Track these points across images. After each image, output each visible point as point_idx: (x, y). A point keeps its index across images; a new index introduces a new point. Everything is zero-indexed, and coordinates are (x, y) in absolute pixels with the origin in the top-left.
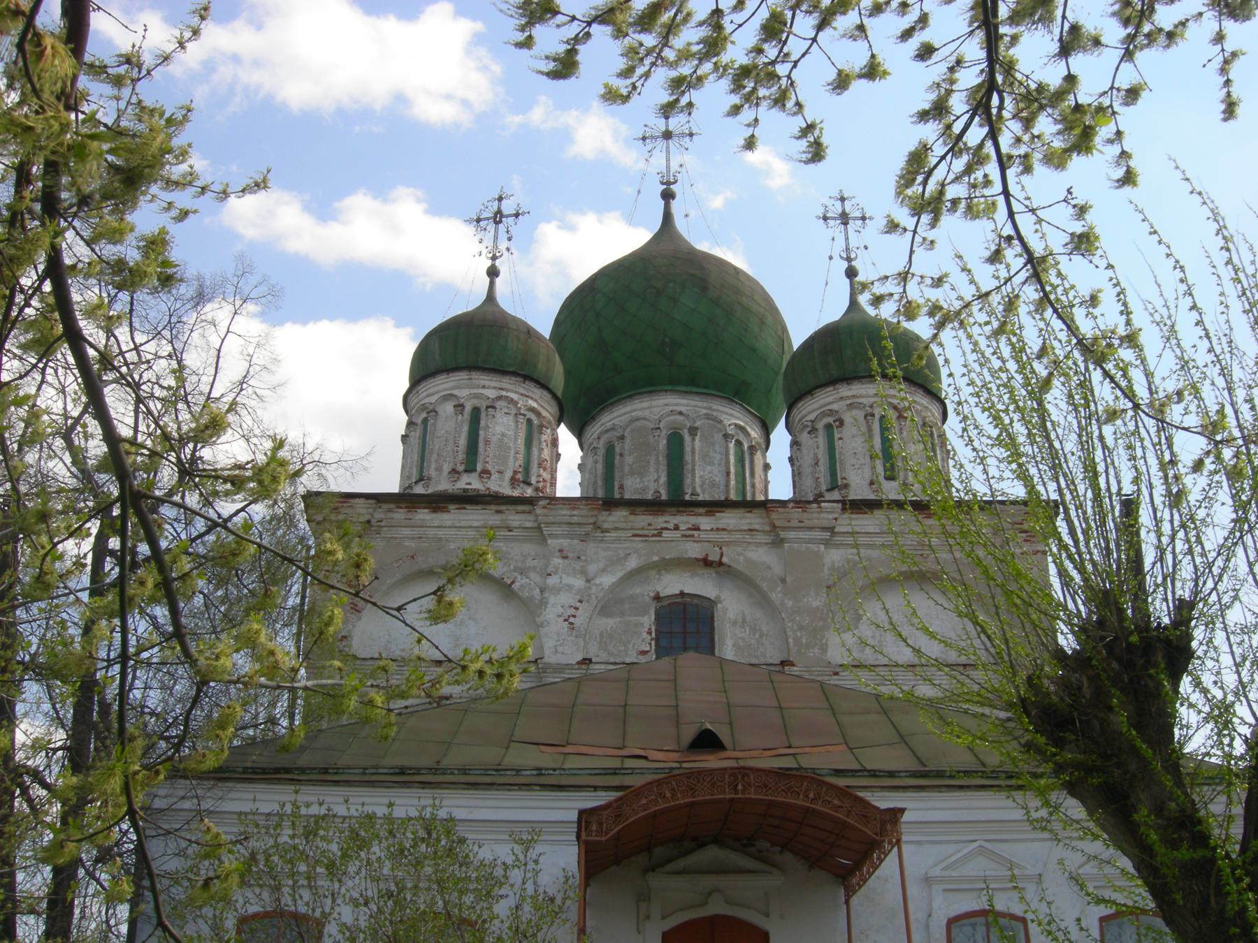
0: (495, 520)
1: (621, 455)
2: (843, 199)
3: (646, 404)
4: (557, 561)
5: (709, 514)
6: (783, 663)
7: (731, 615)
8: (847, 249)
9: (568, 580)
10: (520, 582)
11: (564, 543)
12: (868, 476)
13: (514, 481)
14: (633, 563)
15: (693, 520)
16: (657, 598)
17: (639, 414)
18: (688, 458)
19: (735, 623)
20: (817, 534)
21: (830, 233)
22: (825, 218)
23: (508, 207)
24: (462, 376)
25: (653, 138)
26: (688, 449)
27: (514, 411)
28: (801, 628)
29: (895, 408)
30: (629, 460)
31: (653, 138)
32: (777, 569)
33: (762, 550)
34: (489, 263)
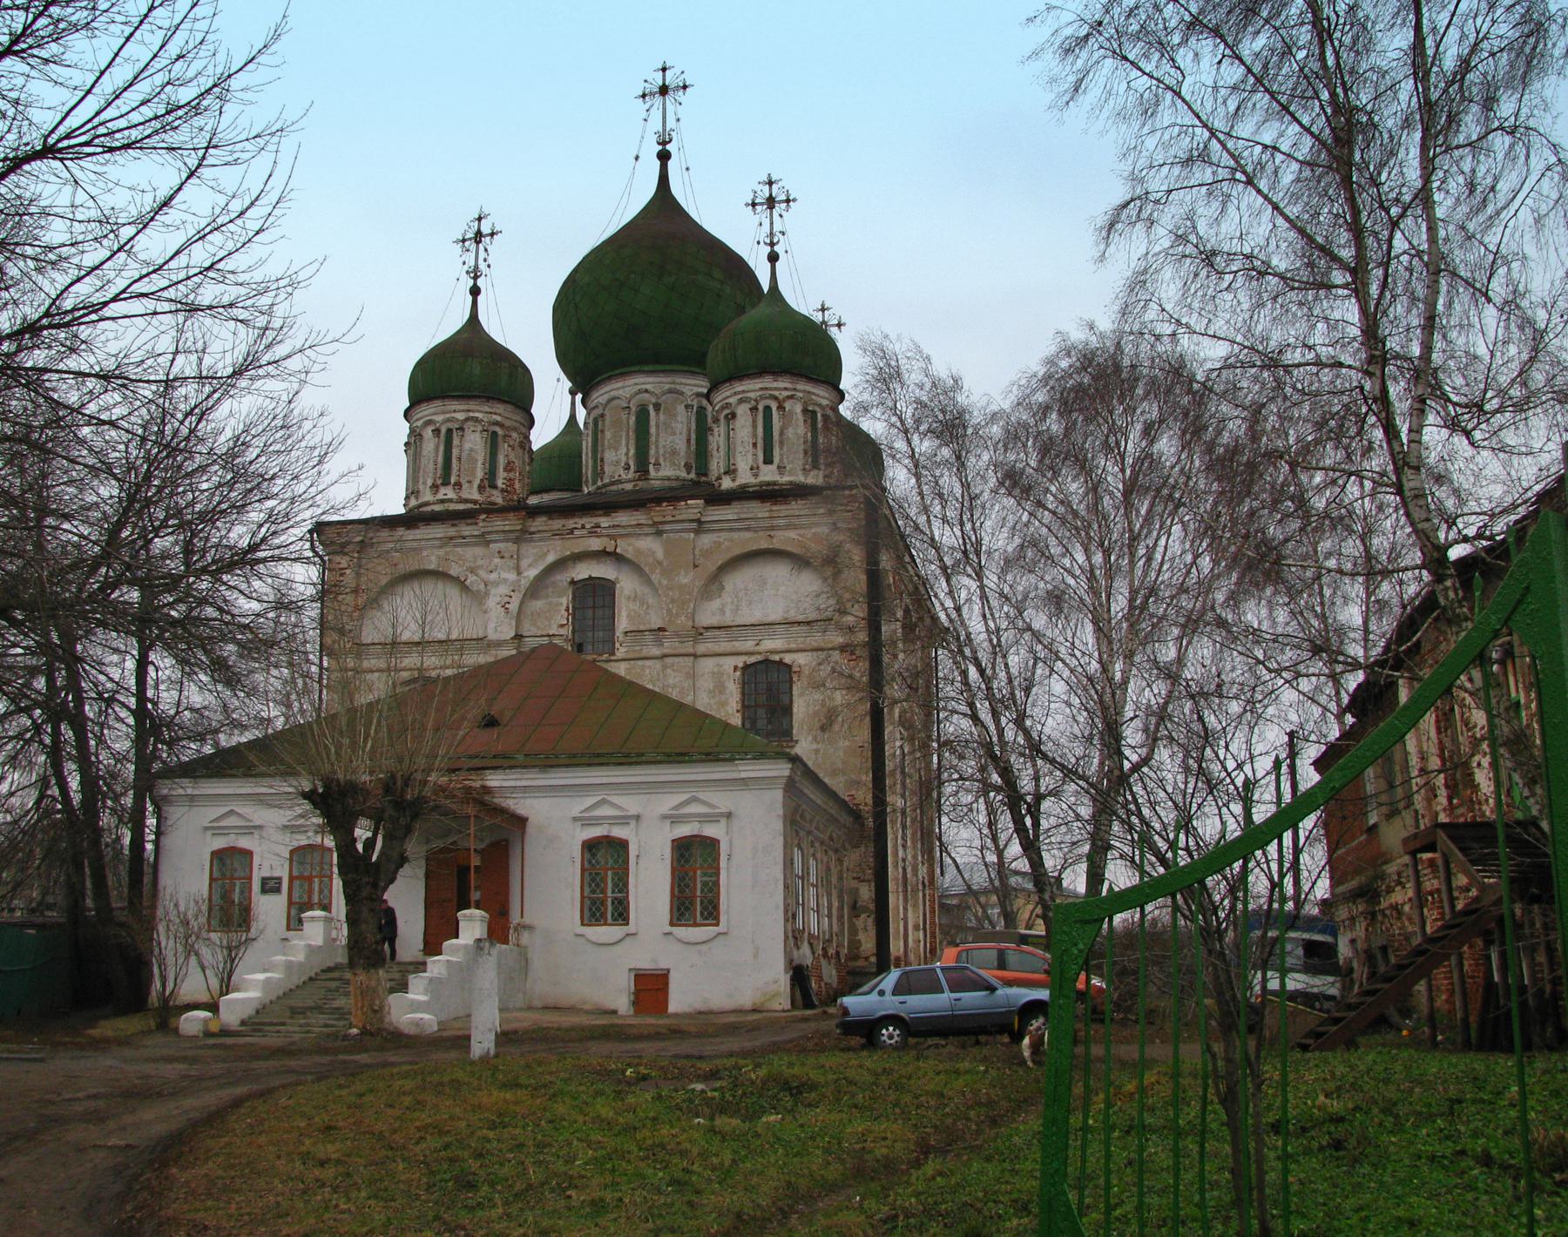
0: (452, 531)
1: (755, 445)
2: (770, 183)
3: (620, 384)
4: (497, 560)
5: (607, 514)
6: (660, 629)
7: (626, 592)
8: (772, 234)
9: (505, 575)
10: (471, 579)
11: (501, 546)
12: (750, 462)
13: (481, 488)
14: (551, 558)
15: (596, 520)
16: (573, 582)
17: (613, 394)
18: (653, 430)
19: (629, 598)
20: (686, 525)
21: (756, 219)
22: (754, 205)
23: (486, 229)
24: (438, 403)
25: (652, 94)
26: (653, 422)
27: (479, 428)
28: (673, 601)
29: (776, 398)
30: (608, 435)
31: (652, 94)
32: (660, 554)
33: (649, 539)
34: (471, 282)
